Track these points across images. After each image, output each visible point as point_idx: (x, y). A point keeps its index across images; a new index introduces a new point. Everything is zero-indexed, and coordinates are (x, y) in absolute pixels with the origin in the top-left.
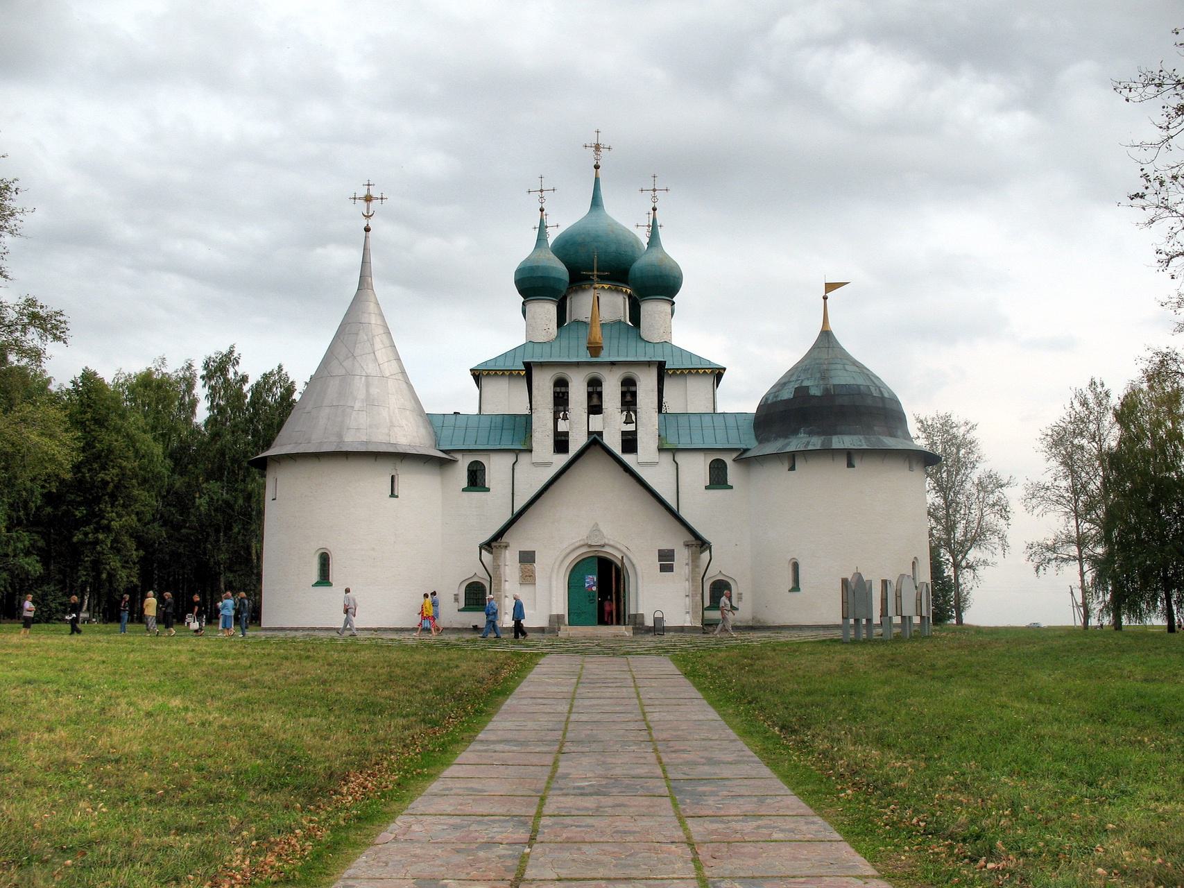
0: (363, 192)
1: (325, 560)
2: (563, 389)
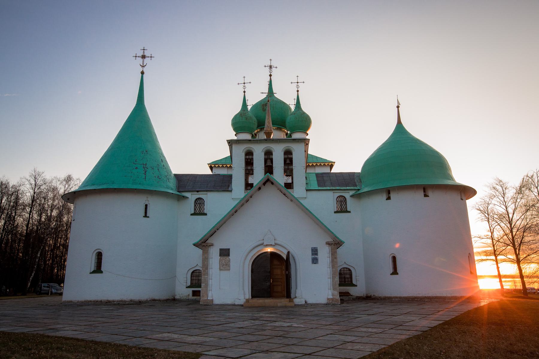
1: (99, 255)
2: (250, 157)
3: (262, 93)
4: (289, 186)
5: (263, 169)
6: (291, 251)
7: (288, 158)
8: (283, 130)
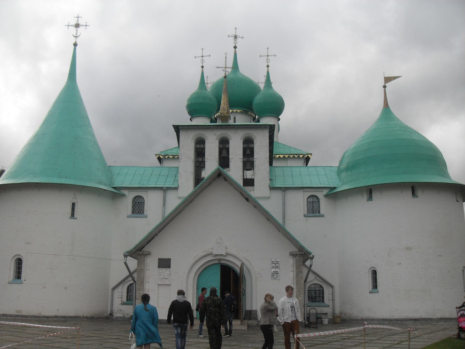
0: (74, 22)
2: (202, 146)
3: (218, 67)
4: (249, 182)
5: (268, 161)
6: (247, 263)
7: (248, 147)
8: (250, 114)
